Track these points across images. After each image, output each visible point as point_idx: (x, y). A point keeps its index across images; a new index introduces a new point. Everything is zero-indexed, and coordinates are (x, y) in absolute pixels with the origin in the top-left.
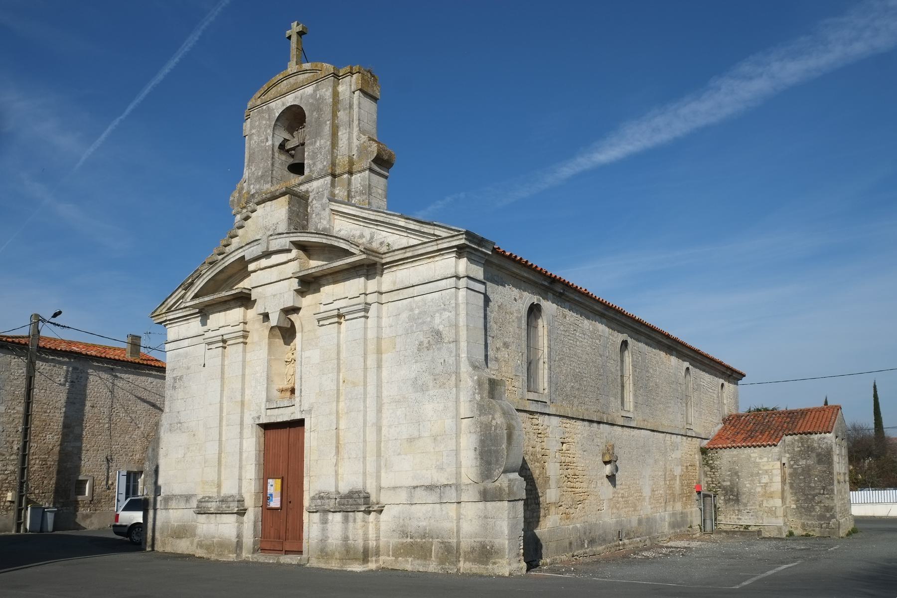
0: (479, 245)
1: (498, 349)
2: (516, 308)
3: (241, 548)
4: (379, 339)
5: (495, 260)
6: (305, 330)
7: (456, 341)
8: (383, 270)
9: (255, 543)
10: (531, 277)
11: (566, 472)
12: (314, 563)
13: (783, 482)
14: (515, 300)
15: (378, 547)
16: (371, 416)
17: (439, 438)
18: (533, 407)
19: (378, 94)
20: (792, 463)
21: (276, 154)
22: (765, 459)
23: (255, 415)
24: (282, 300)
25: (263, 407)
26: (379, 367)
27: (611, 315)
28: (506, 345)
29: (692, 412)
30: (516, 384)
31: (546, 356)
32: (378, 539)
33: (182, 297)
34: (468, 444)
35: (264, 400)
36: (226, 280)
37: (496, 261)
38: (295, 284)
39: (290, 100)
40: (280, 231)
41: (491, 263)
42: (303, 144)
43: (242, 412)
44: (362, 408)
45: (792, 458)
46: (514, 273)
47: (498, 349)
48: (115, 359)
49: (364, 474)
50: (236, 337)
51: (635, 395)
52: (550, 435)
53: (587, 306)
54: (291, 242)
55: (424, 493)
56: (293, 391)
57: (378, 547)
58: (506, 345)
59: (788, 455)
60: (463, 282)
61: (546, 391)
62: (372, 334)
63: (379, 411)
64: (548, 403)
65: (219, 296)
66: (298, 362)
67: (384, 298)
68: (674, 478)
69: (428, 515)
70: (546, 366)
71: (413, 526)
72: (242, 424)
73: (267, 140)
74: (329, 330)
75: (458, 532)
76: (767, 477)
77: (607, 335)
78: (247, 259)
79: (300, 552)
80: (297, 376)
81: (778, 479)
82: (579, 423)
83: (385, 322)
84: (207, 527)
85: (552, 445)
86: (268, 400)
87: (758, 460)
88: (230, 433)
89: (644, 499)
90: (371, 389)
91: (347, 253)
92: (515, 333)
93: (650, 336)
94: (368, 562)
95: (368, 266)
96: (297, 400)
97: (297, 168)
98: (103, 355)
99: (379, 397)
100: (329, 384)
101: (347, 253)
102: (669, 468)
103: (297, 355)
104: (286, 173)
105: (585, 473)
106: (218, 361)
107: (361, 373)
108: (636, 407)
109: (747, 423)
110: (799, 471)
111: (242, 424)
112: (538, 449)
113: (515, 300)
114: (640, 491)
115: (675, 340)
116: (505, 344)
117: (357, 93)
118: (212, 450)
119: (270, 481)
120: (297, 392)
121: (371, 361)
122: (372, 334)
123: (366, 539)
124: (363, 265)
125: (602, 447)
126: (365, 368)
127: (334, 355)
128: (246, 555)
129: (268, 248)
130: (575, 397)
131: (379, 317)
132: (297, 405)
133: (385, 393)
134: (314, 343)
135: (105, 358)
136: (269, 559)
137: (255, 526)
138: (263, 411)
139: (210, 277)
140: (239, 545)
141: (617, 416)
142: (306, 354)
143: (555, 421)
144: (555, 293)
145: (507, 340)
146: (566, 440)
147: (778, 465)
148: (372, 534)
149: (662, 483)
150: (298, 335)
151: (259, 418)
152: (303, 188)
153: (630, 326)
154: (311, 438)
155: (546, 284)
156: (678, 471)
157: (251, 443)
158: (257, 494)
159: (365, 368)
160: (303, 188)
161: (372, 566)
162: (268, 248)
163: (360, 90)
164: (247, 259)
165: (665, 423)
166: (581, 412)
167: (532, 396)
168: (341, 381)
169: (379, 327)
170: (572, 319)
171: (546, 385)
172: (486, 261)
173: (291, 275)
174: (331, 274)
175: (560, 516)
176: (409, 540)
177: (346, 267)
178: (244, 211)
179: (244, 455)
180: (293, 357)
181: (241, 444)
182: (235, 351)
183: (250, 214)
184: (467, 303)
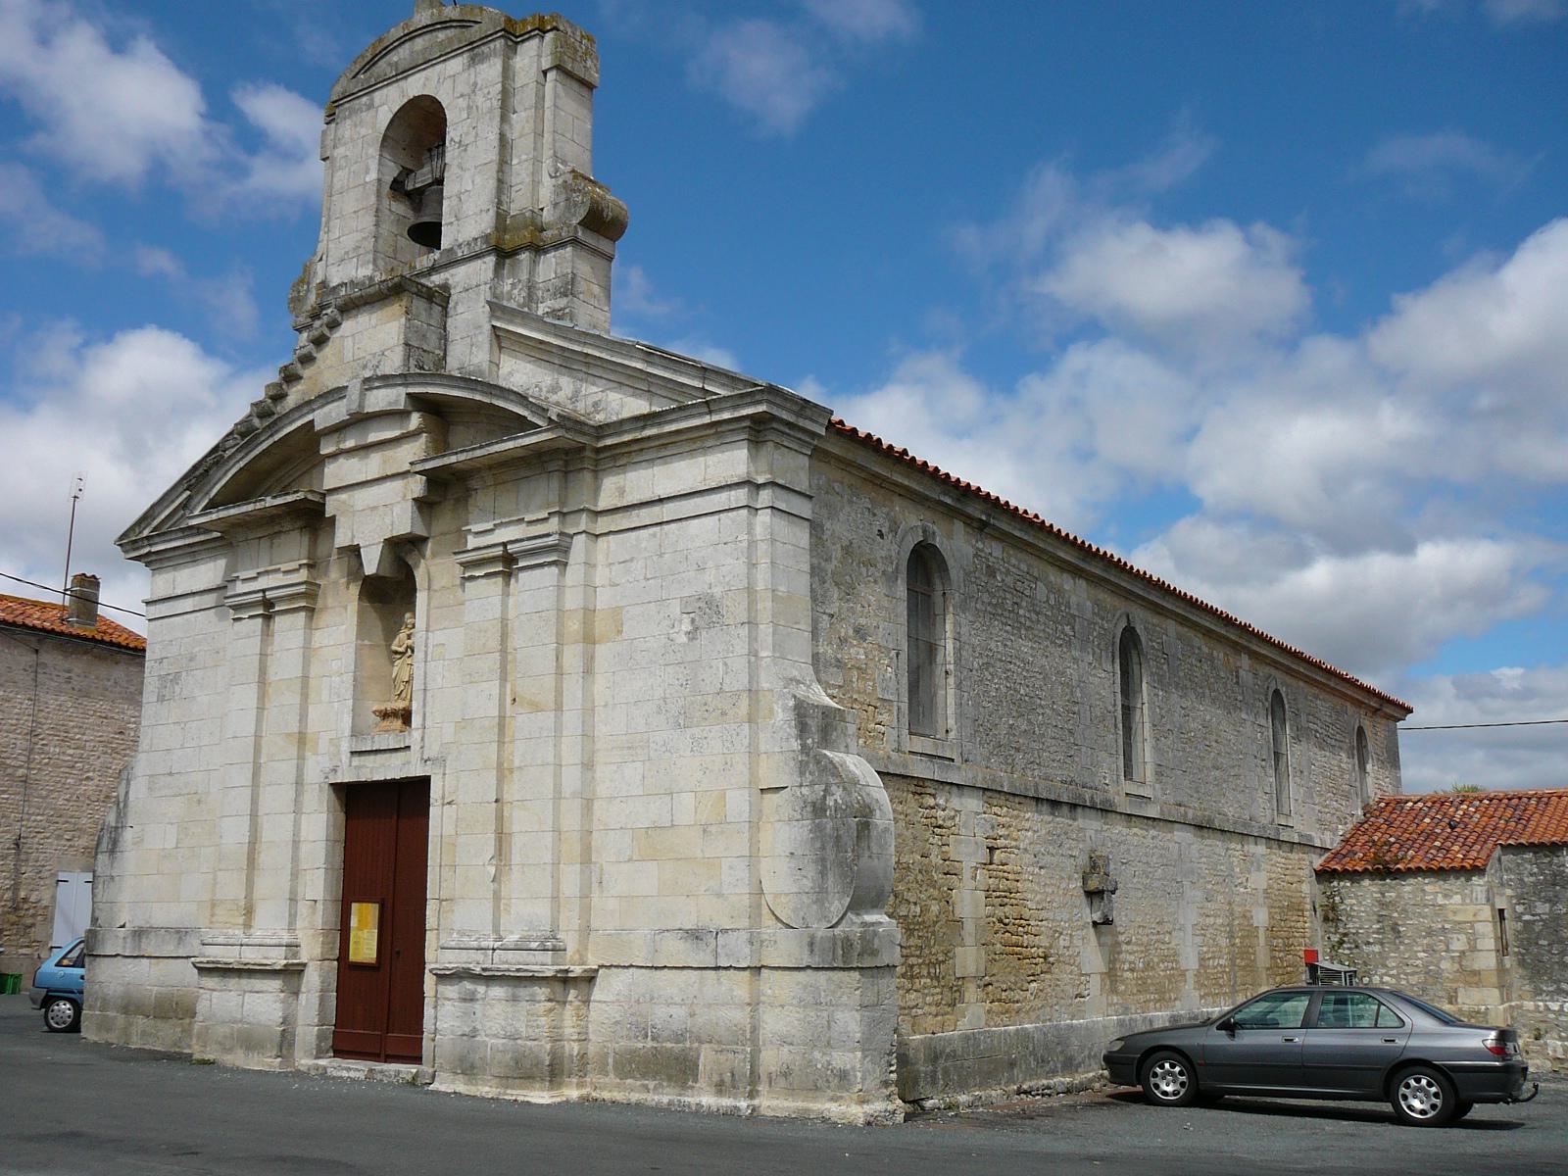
0: (798, 415)
1: (843, 641)
2: (883, 553)
3: (291, 1045)
4: (589, 613)
5: (835, 448)
6: (435, 586)
7: (752, 623)
8: (597, 462)
9: (320, 1037)
10: (914, 486)
11: (1000, 912)
12: (444, 1084)
13: (1503, 950)
14: (881, 535)
15: (583, 1056)
16: (572, 778)
17: (713, 829)
18: (920, 769)
19: (594, 77)
20: (1520, 909)
21: (386, 202)
22: (1457, 898)
23: (328, 765)
24: (388, 521)
25: (346, 747)
26: (588, 671)
27: (1098, 572)
28: (860, 633)
29: (1294, 790)
30: (884, 718)
31: (950, 658)
32: (583, 1039)
33: (184, 506)
34: (784, 835)
35: (347, 732)
36: (269, 473)
37: (835, 450)
38: (417, 486)
39: (415, 86)
40: (389, 371)
41: (827, 453)
42: (440, 182)
43: (301, 757)
44: (551, 759)
45: (1520, 898)
46: (876, 476)
47: (843, 641)
48: (43, 630)
49: (555, 898)
50: (292, 597)
51: (1157, 749)
52: (963, 831)
53: (1043, 551)
54: (408, 394)
55: (682, 946)
56: (406, 717)
57: (583, 1056)
58: (860, 633)
59: (1509, 892)
60: (765, 497)
61: (952, 735)
62: (573, 600)
63: (588, 765)
64: (958, 761)
65: (259, 506)
66: (419, 655)
67: (603, 524)
68: (1251, 932)
69: (679, 1002)
70: (951, 680)
71: (659, 1015)
72: (299, 783)
73: (367, 172)
74: (486, 592)
75: (754, 1029)
76: (1463, 937)
77: (1088, 615)
78: (317, 428)
79: (417, 1059)
80: (417, 684)
81: (1488, 943)
82: (708, 972)
83: (601, 576)
84: (221, 1002)
85: (967, 852)
86: (356, 733)
87: (1440, 900)
88: (276, 798)
89: (1183, 974)
90: (572, 720)
91: (523, 425)
92: (880, 608)
93: (1186, 619)
94: (560, 1085)
95: (567, 452)
96: (416, 735)
97: (427, 234)
98: (19, 620)
99: (588, 736)
100: (484, 701)
101: (523, 425)
102: (1238, 909)
103: (418, 640)
104: (405, 242)
105: (1043, 914)
106: (254, 645)
107: (549, 682)
108: (1159, 774)
109: (1418, 816)
110: (1538, 927)
111: (299, 783)
112: (935, 859)
113: (881, 535)
114: (1173, 957)
115: (1244, 629)
116: (857, 631)
117: (551, 75)
118: (235, 833)
119: (355, 906)
120: (416, 720)
121: (573, 656)
122: (573, 600)
123: (556, 1039)
124: (557, 450)
125: (1083, 860)
126: (559, 672)
127: (494, 643)
128: (304, 1062)
129: (361, 405)
130: (1018, 750)
131: (589, 565)
132: (415, 747)
133: (601, 730)
134: (452, 612)
135: (24, 625)
136: (355, 1069)
137: (322, 1000)
138: (345, 757)
139: (242, 464)
140: (285, 1042)
141: (1118, 792)
142: (437, 637)
143: (972, 803)
144: (969, 521)
145: (863, 621)
146: (1001, 842)
147: (1486, 913)
148: (569, 1029)
149: (1224, 942)
150: (421, 598)
151: (335, 770)
152: (437, 279)
153: (1139, 597)
154: (440, 820)
155: (948, 501)
156: (1261, 917)
157: (320, 826)
158: (326, 932)
159: (559, 672)
160: (437, 279)
161: (573, 1093)
162: (361, 405)
163: (558, 67)
164: (317, 428)
165: (1230, 811)
166: (1030, 780)
167: (920, 744)
168: (509, 700)
169: (590, 587)
170: (1009, 580)
171: (951, 722)
172: (816, 449)
173: (407, 467)
174: (490, 468)
175: (988, 1005)
176: (650, 1044)
177: (522, 453)
178: (317, 323)
179: (304, 848)
180: (409, 642)
181: (297, 825)
182: (289, 628)
183: (327, 332)
184: (773, 541)
